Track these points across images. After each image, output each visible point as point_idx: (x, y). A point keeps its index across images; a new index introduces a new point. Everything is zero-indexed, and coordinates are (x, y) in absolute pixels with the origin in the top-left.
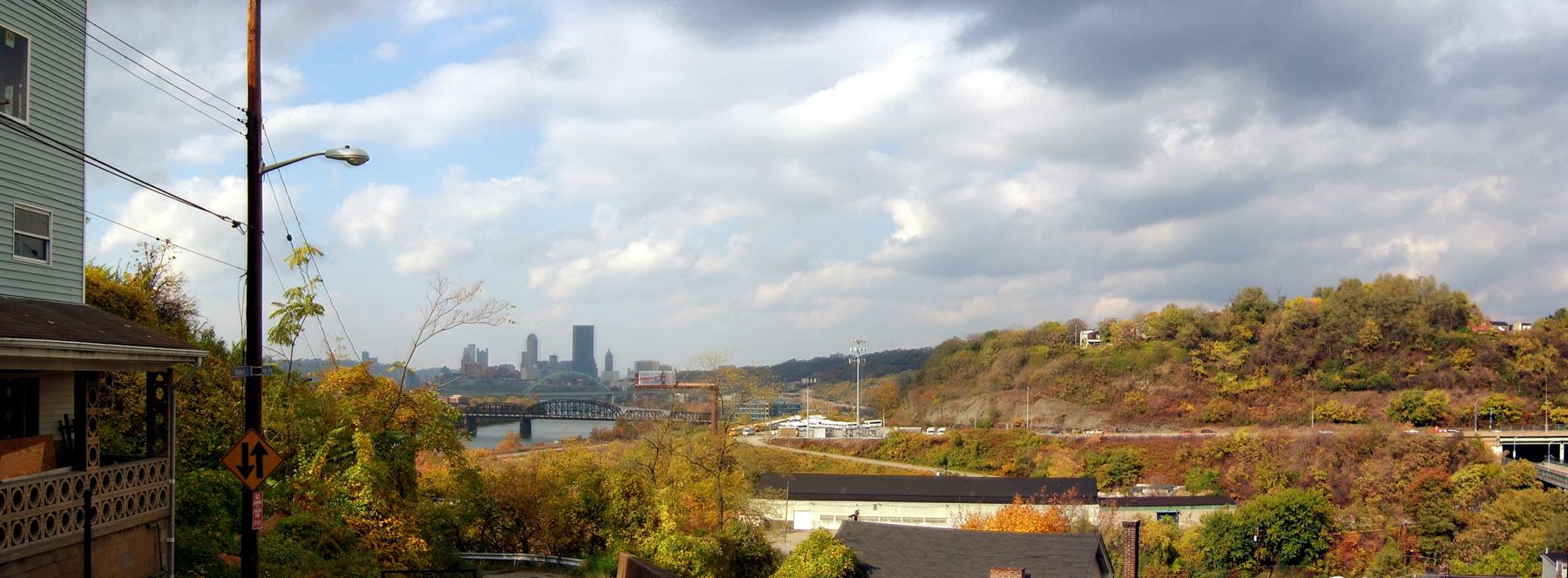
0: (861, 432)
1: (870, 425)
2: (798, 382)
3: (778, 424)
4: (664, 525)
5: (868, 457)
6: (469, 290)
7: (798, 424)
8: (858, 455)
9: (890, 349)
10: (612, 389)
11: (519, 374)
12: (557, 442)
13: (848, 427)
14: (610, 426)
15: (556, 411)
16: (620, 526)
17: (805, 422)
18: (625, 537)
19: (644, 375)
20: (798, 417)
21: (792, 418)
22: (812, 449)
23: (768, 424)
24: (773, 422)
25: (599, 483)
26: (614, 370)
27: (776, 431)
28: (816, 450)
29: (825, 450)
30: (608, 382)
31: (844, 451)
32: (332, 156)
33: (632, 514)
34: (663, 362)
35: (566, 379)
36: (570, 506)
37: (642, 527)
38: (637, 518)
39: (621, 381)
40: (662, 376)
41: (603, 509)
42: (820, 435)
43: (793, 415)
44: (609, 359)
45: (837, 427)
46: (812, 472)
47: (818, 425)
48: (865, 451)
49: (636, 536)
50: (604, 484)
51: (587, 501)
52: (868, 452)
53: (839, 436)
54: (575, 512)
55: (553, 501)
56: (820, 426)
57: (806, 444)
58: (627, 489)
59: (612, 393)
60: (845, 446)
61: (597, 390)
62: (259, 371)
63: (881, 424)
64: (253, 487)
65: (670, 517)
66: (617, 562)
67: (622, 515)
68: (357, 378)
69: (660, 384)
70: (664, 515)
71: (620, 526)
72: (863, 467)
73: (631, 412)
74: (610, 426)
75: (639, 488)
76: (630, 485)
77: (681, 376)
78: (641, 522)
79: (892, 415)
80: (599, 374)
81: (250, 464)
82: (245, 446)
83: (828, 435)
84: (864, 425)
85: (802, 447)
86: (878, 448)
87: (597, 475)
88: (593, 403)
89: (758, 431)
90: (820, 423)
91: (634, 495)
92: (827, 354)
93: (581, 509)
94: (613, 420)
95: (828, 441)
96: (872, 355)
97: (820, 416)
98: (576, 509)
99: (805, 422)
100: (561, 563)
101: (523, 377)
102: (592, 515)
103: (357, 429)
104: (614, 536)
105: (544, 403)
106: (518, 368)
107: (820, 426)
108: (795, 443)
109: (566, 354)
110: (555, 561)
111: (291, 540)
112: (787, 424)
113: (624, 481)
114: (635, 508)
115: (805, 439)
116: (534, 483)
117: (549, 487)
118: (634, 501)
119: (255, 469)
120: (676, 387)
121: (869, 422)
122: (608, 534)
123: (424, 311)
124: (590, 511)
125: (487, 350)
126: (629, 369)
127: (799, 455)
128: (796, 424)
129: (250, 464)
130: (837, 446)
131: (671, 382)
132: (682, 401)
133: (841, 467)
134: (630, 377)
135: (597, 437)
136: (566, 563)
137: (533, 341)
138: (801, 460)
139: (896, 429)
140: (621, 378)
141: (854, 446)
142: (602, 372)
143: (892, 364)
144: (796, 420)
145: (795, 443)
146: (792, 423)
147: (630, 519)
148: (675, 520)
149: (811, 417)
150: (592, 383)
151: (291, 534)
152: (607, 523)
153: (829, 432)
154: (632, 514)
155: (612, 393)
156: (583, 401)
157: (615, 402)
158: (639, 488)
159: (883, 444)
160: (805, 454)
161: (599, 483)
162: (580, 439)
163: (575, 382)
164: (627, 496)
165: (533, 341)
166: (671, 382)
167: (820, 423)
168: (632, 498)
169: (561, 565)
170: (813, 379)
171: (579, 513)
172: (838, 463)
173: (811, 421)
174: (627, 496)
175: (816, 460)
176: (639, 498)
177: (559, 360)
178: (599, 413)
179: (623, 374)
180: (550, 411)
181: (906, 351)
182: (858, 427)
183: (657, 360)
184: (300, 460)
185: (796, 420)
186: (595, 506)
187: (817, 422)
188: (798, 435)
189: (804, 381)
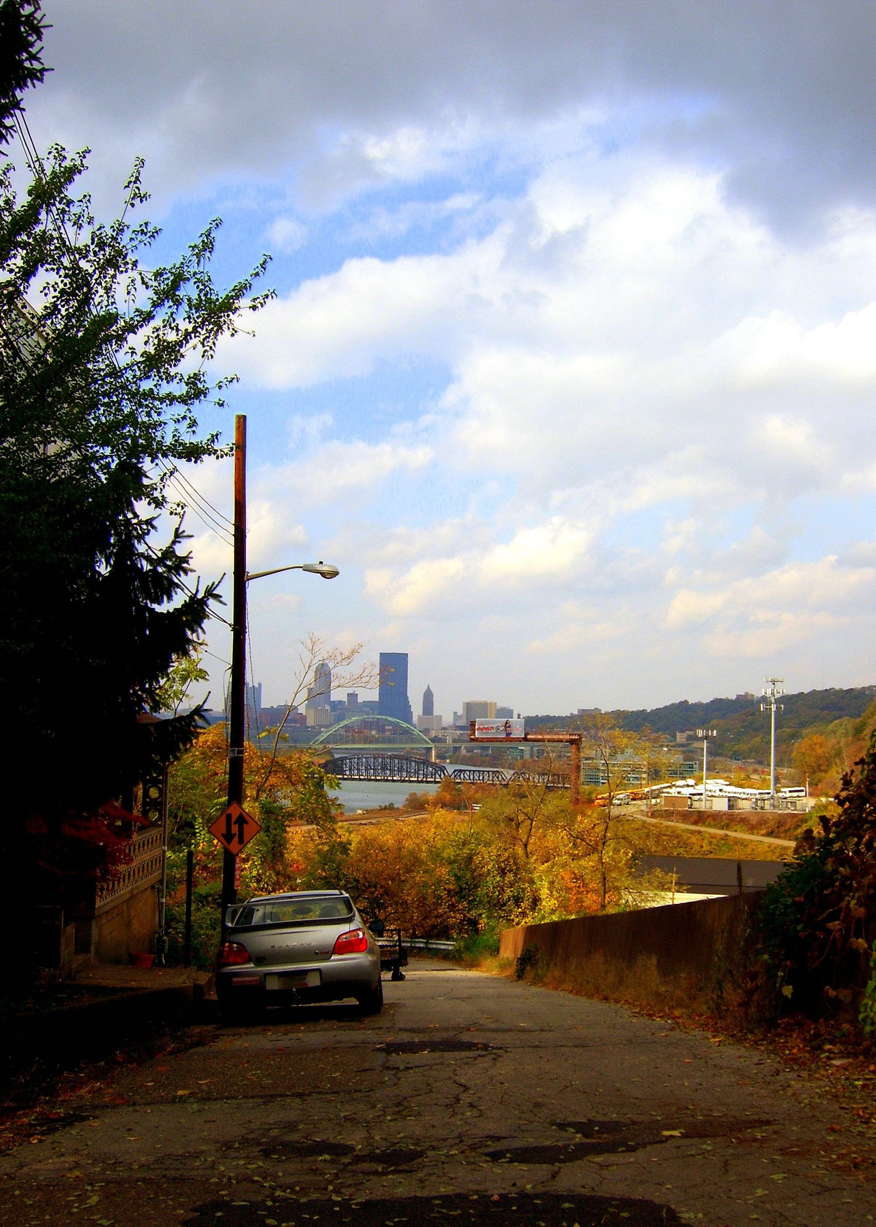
0: (776, 803)
1: (788, 795)
2: (692, 733)
3: (660, 791)
4: (544, 903)
5: (785, 839)
6: (346, 653)
7: (691, 790)
8: (770, 834)
9: (821, 686)
10: (434, 740)
11: (303, 718)
12: (360, 812)
13: (758, 796)
14: (432, 790)
15: (358, 770)
16: (495, 905)
17: (700, 788)
18: (500, 917)
19: (482, 724)
20: (691, 782)
21: (681, 783)
22: (709, 826)
23: (646, 790)
24: (654, 788)
25: (470, 859)
26: (435, 714)
27: (658, 800)
28: (715, 826)
29: (727, 827)
30: (426, 731)
31: (752, 828)
32: (308, 569)
33: (508, 892)
34: (501, 704)
35: (367, 724)
36: (439, 881)
37: (519, 906)
38: (514, 896)
39: (444, 729)
40: (507, 725)
41: (476, 887)
42: (721, 805)
43: (684, 778)
44: (428, 697)
45: (744, 796)
46: (709, 856)
47: (718, 793)
48: (782, 829)
49: (512, 917)
50: (477, 859)
51: (458, 878)
52: (786, 831)
53: (745, 806)
54: (445, 889)
55: (419, 877)
56: (721, 794)
57: (701, 817)
58: (503, 865)
59: (431, 745)
60: (754, 822)
61: (413, 741)
62: (241, 752)
63: (803, 794)
64: (235, 852)
65: (551, 895)
66: (499, 941)
67: (497, 893)
68: (213, 742)
69: (504, 736)
70: (544, 892)
71: (495, 905)
72: (778, 851)
73: (461, 771)
74: (432, 790)
75: (515, 863)
76: (506, 860)
77: (532, 723)
78: (517, 901)
79: (820, 781)
80: (415, 719)
81: (233, 832)
82: (229, 817)
83: (730, 807)
84: (780, 795)
85: (696, 823)
86: (799, 826)
87: (469, 849)
88: (408, 759)
89: (633, 799)
90: (721, 790)
91: (510, 871)
92: (730, 694)
93: (452, 887)
94: (439, 782)
95: (732, 815)
96: (793, 697)
97: (721, 781)
98: (446, 887)
99: (700, 788)
100: (430, 946)
101: (310, 722)
102: (464, 893)
103: (248, 799)
104: (488, 917)
105: (342, 759)
106: (302, 710)
107: (721, 794)
108: (685, 817)
109: (370, 694)
110: (422, 945)
111: (209, 909)
112: (673, 791)
113: (500, 855)
114: (511, 885)
115: (699, 812)
116: (399, 858)
117: (415, 862)
118: (510, 877)
119: (237, 836)
120: (525, 739)
121: (787, 790)
122: (480, 915)
123: (298, 674)
124: (462, 889)
125: (260, 684)
126: (455, 713)
127: (693, 832)
128: (686, 792)
129: (233, 832)
130: (743, 821)
131: (518, 732)
132: (527, 756)
133: (749, 851)
134: (458, 724)
135: (417, 805)
136: (434, 946)
137: (323, 674)
138: (693, 839)
139: (823, 799)
140: (444, 725)
141: (766, 822)
142: (419, 717)
143: (823, 709)
144: (688, 786)
145: (685, 817)
146: (682, 788)
147: (506, 898)
148: (556, 899)
149: (708, 781)
150: (407, 732)
151: (208, 903)
152: (480, 902)
153: (732, 801)
154: (508, 892)
155: (431, 745)
156: (396, 757)
157: (437, 757)
158: (515, 863)
159: (806, 821)
160: (700, 832)
161: (470, 859)
162: (389, 809)
163: (381, 729)
164: (503, 872)
165: (323, 674)
166: (518, 732)
167: (721, 790)
168: (508, 874)
169: (430, 949)
170: (712, 731)
171: (449, 891)
172: (744, 844)
173: (708, 787)
174: (503, 872)
175: (714, 841)
176: (516, 874)
177: (360, 700)
178: (417, 773)
179: (448, 720)
180: (350, 770)
181: (841, 691)
182: (772, 796)
183: (493, 701)
184: (197, 831)
185: (688, 786)
186: (467, 883)
187: (717, 788)
188: (691, 806)
189: (700, 733)
